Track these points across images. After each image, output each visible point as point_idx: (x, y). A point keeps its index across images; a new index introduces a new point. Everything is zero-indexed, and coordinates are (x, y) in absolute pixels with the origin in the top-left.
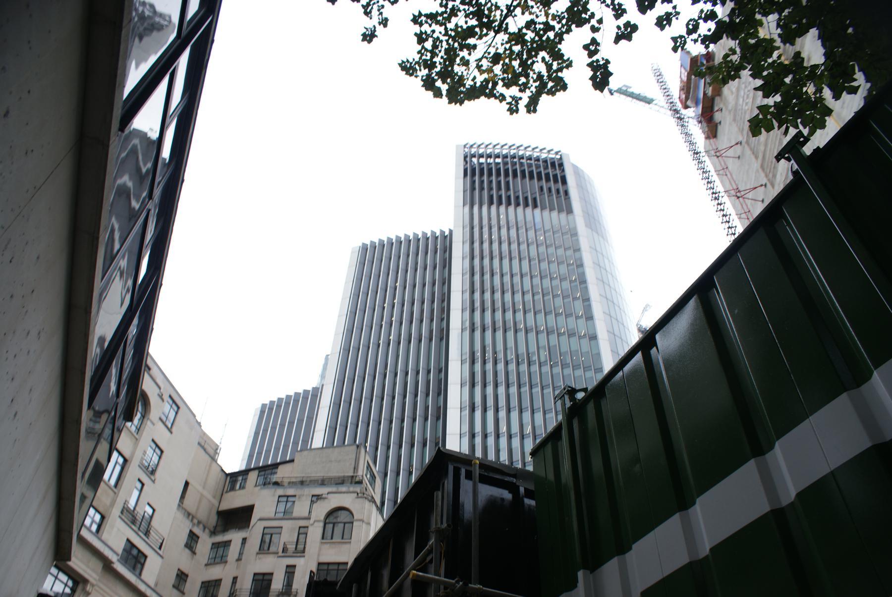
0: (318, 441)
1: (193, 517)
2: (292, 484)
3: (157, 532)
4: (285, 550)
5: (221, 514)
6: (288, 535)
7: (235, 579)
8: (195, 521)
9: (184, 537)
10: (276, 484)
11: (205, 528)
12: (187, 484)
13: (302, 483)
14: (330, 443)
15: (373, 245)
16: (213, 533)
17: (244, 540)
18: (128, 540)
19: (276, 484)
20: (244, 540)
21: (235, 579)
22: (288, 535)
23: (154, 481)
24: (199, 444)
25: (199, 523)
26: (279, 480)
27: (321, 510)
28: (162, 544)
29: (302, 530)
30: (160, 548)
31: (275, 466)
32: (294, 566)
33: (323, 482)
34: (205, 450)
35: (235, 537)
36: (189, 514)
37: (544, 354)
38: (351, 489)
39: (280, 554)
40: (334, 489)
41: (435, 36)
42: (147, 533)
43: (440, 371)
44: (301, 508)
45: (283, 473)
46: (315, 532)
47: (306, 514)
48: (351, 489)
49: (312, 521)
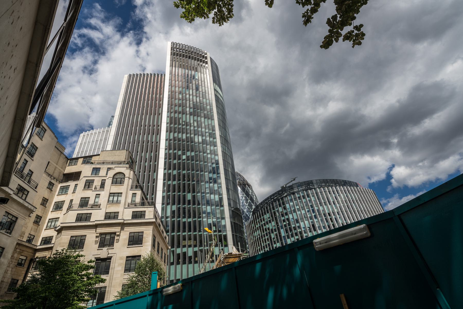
0: (109, 147)
1: (51, 176)
2: (99, 163)
3: (34, 181)
4: (95, 188)
5: (65, 175)
6: (97, 182)
7: (72, 201)
8: (52, 178)
9: (47, 184)
10: (92, 163)
11: (57, 180)
12: (49, 162)
13: (103, 163)
14: (114, 149)
15: (134, 75)
16: (61, 182)
17: (76, 185)
18: (19, 185)
19: (92, 163)
20: (76, 185)
21: (72, 201)
22: (97, 182)
23: (33, 160)
24: (55, 147)
25: (54, 178)
26: (93, 162)
27: (111, 173)
28: (37, 186)
29: (103, 181)
30: (36, 188)
31: (91, 157)
32: (99, 194)
33: (112, 163)
34: (58, 149)
35: (72, 184)
36: (49, 175)
37: (195, 124)
38: (124, 166)
39: (93, 190)
40: (117, 166)
41: (98, 216)
42: (29, 182)
43: (158, 126)
44: (102, 173)
45: (94, 159)
46: (108, 182)
47: (105, 175)
48: (124, 166)
49: (107, 178)
